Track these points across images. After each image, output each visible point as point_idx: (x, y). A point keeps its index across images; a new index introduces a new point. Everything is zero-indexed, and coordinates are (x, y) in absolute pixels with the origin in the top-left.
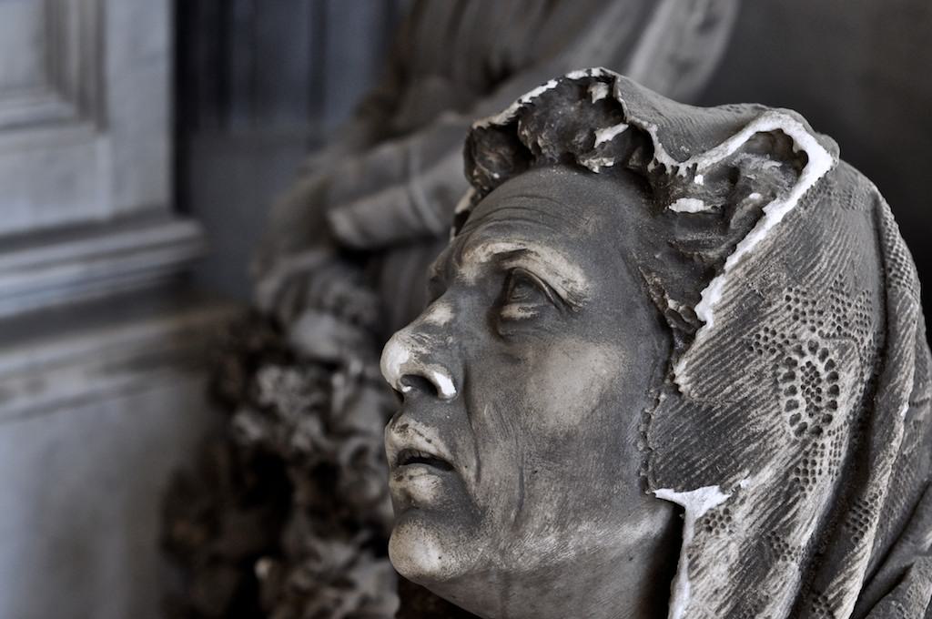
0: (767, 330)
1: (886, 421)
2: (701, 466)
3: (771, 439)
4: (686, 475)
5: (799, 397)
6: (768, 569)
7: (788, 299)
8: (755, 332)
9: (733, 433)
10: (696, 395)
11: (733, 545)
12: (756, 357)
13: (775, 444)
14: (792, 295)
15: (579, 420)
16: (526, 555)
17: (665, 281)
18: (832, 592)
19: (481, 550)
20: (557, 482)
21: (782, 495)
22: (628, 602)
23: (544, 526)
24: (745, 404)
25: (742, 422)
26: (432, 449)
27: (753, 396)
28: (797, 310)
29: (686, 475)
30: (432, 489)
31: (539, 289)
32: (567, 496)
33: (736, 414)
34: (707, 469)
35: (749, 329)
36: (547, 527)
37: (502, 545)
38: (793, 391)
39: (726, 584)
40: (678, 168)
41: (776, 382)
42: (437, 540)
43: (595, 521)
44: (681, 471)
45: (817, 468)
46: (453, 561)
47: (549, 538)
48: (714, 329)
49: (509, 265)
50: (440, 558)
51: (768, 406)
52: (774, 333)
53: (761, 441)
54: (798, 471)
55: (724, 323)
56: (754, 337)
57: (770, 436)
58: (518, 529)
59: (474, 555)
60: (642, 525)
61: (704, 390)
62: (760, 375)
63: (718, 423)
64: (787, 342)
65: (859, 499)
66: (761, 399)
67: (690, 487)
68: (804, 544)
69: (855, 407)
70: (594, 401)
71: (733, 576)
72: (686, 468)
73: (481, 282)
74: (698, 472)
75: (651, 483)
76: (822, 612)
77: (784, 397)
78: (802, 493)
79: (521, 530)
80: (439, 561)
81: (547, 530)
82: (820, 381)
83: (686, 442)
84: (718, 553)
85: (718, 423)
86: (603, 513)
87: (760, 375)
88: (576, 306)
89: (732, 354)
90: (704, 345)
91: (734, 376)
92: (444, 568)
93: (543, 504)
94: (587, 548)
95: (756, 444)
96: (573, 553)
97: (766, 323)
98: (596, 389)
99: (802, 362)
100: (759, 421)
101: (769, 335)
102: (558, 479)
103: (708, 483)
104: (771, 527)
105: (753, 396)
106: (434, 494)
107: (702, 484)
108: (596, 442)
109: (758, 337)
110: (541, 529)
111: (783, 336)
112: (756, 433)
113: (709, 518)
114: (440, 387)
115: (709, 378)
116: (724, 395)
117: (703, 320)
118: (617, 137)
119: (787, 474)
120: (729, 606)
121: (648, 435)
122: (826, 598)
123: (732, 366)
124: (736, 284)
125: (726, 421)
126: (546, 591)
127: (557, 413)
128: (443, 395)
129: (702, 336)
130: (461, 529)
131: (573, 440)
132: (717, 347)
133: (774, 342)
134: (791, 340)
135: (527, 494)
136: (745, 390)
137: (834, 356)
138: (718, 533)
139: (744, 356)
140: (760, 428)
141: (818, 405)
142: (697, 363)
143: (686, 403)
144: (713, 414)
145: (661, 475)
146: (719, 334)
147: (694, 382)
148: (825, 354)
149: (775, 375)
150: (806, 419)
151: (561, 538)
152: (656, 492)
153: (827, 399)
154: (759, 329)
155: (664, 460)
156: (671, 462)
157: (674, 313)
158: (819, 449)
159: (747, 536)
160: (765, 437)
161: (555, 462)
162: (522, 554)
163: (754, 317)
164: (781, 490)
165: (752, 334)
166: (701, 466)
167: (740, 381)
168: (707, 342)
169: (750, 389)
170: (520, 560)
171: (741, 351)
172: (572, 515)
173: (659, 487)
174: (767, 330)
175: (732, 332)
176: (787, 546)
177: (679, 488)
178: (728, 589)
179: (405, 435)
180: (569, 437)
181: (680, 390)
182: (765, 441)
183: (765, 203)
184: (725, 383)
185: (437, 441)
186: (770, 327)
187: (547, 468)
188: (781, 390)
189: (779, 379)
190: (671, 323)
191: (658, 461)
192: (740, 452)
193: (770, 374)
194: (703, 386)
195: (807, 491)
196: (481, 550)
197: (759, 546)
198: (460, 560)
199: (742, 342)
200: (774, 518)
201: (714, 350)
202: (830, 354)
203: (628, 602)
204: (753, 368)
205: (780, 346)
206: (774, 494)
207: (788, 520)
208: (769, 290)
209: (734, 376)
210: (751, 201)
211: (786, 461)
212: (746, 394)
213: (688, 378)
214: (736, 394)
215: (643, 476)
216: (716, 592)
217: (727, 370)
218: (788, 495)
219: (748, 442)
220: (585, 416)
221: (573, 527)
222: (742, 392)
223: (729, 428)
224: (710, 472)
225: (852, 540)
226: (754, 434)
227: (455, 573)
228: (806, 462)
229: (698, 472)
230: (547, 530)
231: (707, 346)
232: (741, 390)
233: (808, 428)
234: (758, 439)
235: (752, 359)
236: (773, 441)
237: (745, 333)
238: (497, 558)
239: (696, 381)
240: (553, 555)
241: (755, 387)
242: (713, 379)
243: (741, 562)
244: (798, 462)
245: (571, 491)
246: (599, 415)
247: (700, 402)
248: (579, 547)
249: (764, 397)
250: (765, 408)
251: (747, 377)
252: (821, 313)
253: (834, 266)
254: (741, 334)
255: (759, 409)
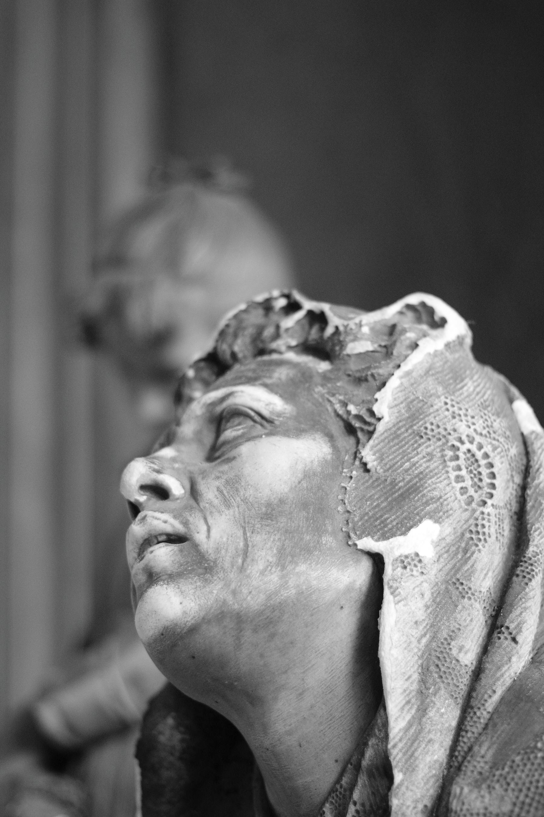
0: (432, 424)
1: (536, 505)
2: (392, 521)
3: (445, 503)
4: (381, 529)
5: (464, 472)
6: (456, 606)
7: (446, 404)
8: (423, 424)
9: (415, 497)
10: (382, 470)
11: (425, 585)
12: (425, 442)
13: (449, 507)
14: (448, 401)
15: (289, 489)
16: (253, 593)
17: (347, 397)
18: (512, 622)
19: (215, 592)
20: (275, 535)
21: (460, 550)
22: (342, 652)
23: (267, 567)
24: (421, 476)
25: (421, 489)
26: (168, 529)
27: (427, 471)
28: (454, 413)
29: (381, 529)
30: (170, 557)
31: (247, 416)
32: (284, 545)
33: (415, 484)
34: (397, 524)
35: (418, 423)
36: (270, 568)
37: (233, 586)
38: (459, 468)
39: (424, 618)
40: (348, 325)
41: (445, 461)
42: (177, 590)
43: (310, 564)
44: (375, 526)
45: (486, 530)
46: (193, 604)
47: (272, 576)
48: (390, 421)
49: (219, 409)
50: (181, 603)
51: (440, 477)
52: (438, 427)
53: (438, 503)
54: (471, 532)
55: (397, 418)
56: (422, 428)
57: (445, 500)
58: (245, 570)
59: (210, 596)
60: (349, 571)
61: (388, 466)
62: (431, 456)
63: (402, 490)
64: (450, 434)
65: (525, 557)
66: (434, 472)
67: (385, 537)
68: (484, 590)
69: (512, 494)
70: (299, 475)
71: (429, 611)
72: (380, 524)
73: (198, 434)
74: (390, 526)
75: (352, 535)
76: (506, 638)
77: (452, 472)
78: (477, 548)
79: (248, 571)
80: (180, 606)
81: (270, 570)
82: (479, 466)
83: (378, 505)
84: (414, 589)
85: (402, 490)
86: (315, 557)
87: (431, 456)
88: (277, 420)
89: (406, 440)
90: (383, 434)
91: (410, 455)
92: (185, 613)
93: (264, 550)
94: (304, 587)
95: (435, 505)
96: (294, 591)
97: (431, 419)
98: (300, 467)
99: (463, 448)
100: (435, 488)
101: (434, 427)
102: (276, 532)
103: (399, 533)
104: (455, 574)
105: (427, 471)
106: (172, 559)
107: (393, 535)
108: (305, 506)
109: (426, 428)
110: (265, 570)
111: (446, 429)
112: (434, 498)
113: (403, 558)
114: (171, 489)
115: (390, 457)
116: (404, 470)
117: (380, 416)
118: (298, 322)
119: (463, 534)
120: (428, 636)
121: (346, 501)
122: (508, 628)
123: (408, 449)
124: (404, 390)
125: (408, 490)
126: (272, 636)
127: (270, 484)
128: (174, 495)
129: (381, 427)
130: (197, 579)
131: (285, 504)
132: (394, 435)
133: (439, 433)
134: (452, 432)
135: (250, 544)
136: (421, 465)
137: (488, 449)
138: (412, 570)
139: (416, 442)
140: (436, 493)
141: (480, 484)
142: (379, 447)
143: (374, 478)
144: (397, 485)
145: (359, 529)
146: (394, 426)
147: (378, 461)
148: (480, 447)
149: (443, 456)
150: (471, 492)
151: (282, 577)
152: (358, 542)
153: (487, 480)
154: (425, 423)
155: (361, 519)
156: (367, 521)
157: (358, 417)
158: (486, 516)
159: (437, 580)
160: (441, 500)
161: (272, 520)
162: (250, 592)
163: (421, 414)
164: (459, 546)
165: (421, 427)
166: (392, 521)
167: (416, 459)
168: (386, 431)
169: (424, 465)
170: (249, 598)
171: (413, 438)
172: (289, 558)
173: (360, 537)
174: (432, 424)
175: (405, 425)
176: (470, 588)
177: (376, 537)
178: (426, 622)
179: (144, 524)
180: (282, 501)
181: (369, 466)
182: (442, 504)
183: (419, 339)
184: (403, 460)
185: (171, 520)
186: (434, 422)
187: (265, 525)
188: (449, 466)
189: (446, 458)
190: (355, 424)
191: (356, 519)
192: (422, 510)
193: (439, 455)
194: (386, 464)
195: (480, 547)
196: (215, 592)
197: (447, 590)
198: (198, 603)
199: (414, 432)
200: (456, 569)
201: (391, 437)
202: (485, 447)
203: (342, 652)
204: (423, 450)
205: (444, 436)
206: (454, 549)
207: (468, 570)
208: (431, 396)
209: (410, 455)
210: (409, 338)
211: (461, 524)
212: (421, 469)
213: (374, 457)
214: (414, 468)
215: (346, 532)
216: (416, 623)
217: (404, 452)
218: (466, 551)
219: (427, 503)
220: (293, 486)
221: (291, 568)
222: (418, 467)
223: (410, 494)
224: (400, 525)
225: (523, 584)
226: (432, 499)
227: (194, 617)
228: (477, 525)
229: (390, 526)
230: (270, 570)
231: (386, 435)
232: (417, 465)
233: (475, 501)
234: (436, 502)
235: (423, 443)
236: (448, 505)
237: (415, 425)
238: (230, 599)
239: (381, 459)
240: (276, 593)
241: (428, 464)
242: (394, 459)
243: (434, 601)
244: (470, 526)
245: (287, 541)
246: (305, 485)
247: (385, 476)
248: (298, 586)
249: (436, 471)
250: (438, 478)
251: (420, 456)
252: (473, 417)
253: (478, 394)
254: (411, 426)
255: (433, 479)
